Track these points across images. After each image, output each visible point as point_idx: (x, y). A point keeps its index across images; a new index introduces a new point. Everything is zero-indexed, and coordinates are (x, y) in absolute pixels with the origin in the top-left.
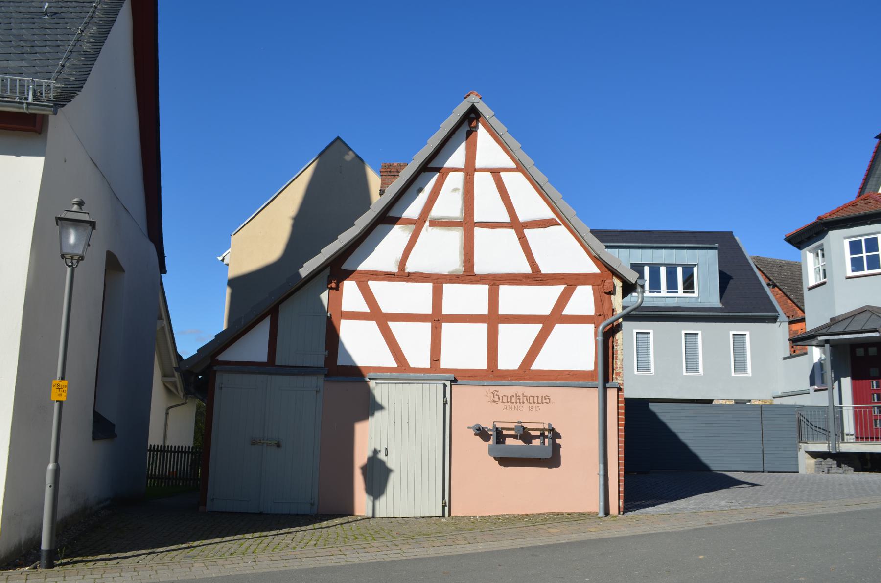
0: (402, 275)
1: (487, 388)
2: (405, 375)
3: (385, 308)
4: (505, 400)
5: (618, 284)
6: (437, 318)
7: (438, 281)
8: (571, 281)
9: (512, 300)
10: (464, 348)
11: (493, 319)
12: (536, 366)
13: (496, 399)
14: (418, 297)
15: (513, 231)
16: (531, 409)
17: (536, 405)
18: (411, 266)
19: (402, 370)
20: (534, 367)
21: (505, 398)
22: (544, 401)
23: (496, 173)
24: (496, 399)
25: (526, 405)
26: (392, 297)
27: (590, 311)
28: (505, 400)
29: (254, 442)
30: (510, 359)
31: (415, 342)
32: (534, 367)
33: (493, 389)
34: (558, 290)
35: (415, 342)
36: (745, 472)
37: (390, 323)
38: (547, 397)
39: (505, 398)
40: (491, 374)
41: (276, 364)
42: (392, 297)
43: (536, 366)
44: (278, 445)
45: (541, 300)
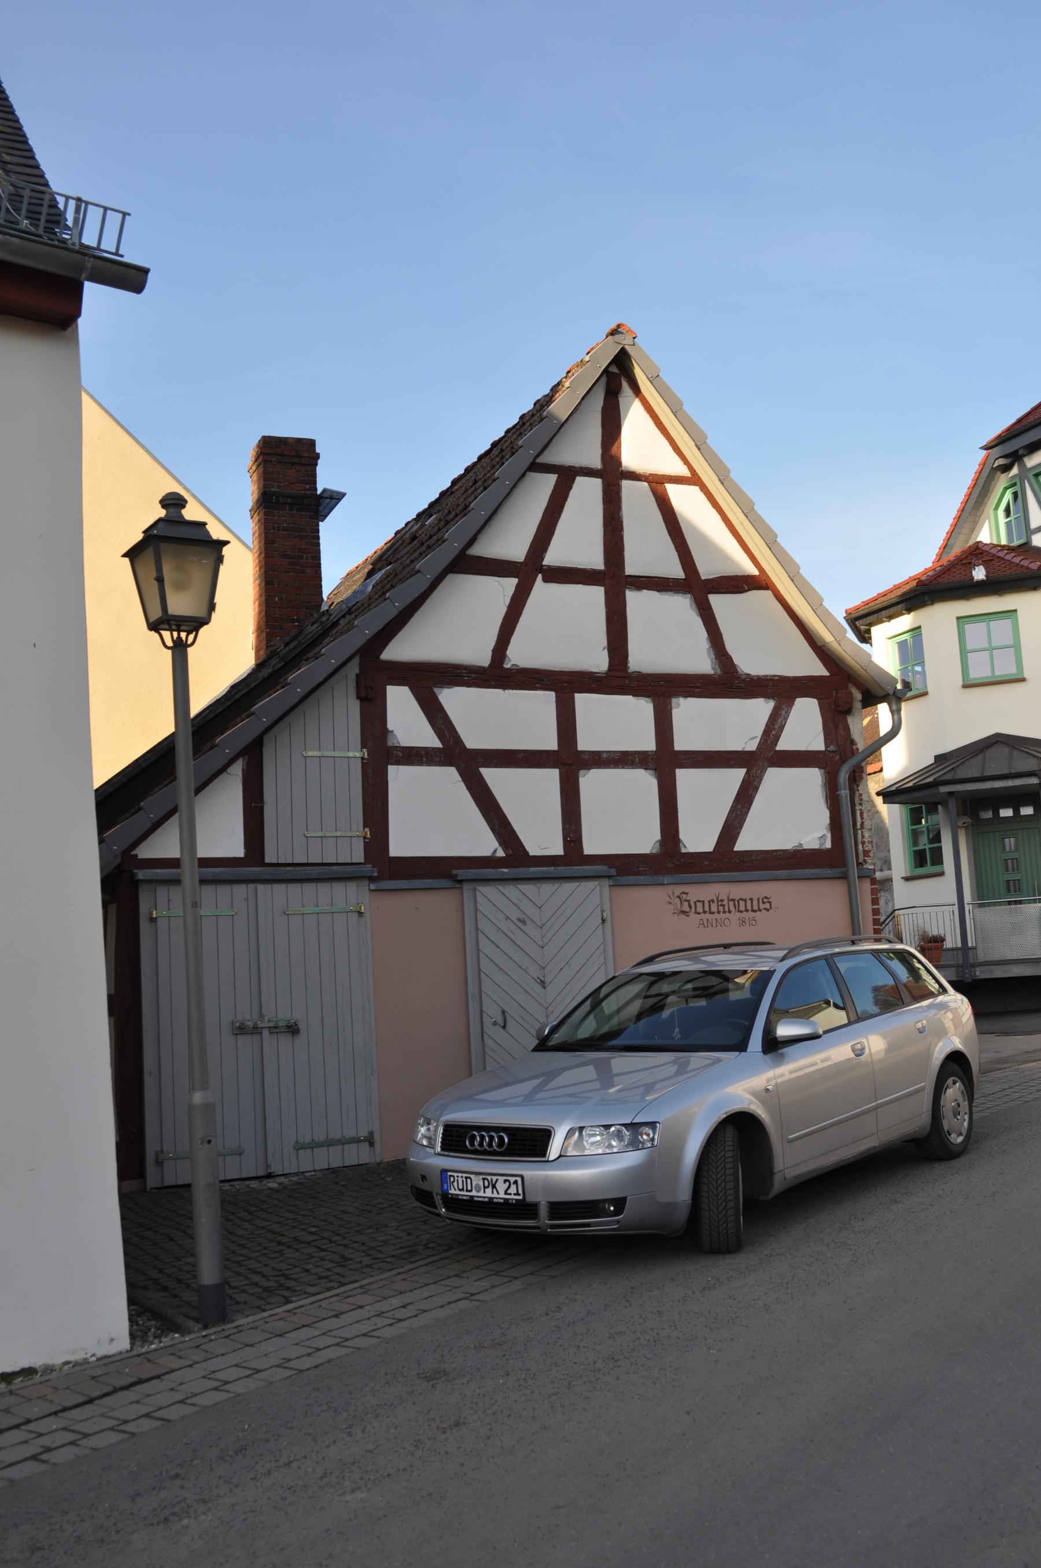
0: (498, 674)
1: (669, 890)
2: (522, 872)
3: (472, 741)
4: (700, 909)
5: (858, 696)
6: (569, 761)
7: (566, 685)
8: (782, 691)
9: (697, 723)
10: (620, 815)
11: (665, 761)
12: (742, 845)
13: (686, 908)
14: (525, 719)
15: (469, 745)
16: (743, 922)
17: (751, 914)
18: (518, 656)
19: (514, 861)
20: (740, 846)
21: (699, 905)
22: (762, 906)
23: (657, 483)
24: (686, 908)
25: (735, 916)
26: (483, 716)
27: (817, 743)
28: (700, 909)
29: (240, 1030)
30: (699, 836)
31: (531, 801)
32: (740, 846)
33: (678, 890)
34: (761, 708)
35: (531, 801)
36: (497, 946)
37: (484, 771)
38: (766, 900)
39: (699, 905)
40: (669, 861)
41: (267, 860)
42: (483, 716)
43: (742, 845)
44: (293, 1030)
45: (739, 722)
